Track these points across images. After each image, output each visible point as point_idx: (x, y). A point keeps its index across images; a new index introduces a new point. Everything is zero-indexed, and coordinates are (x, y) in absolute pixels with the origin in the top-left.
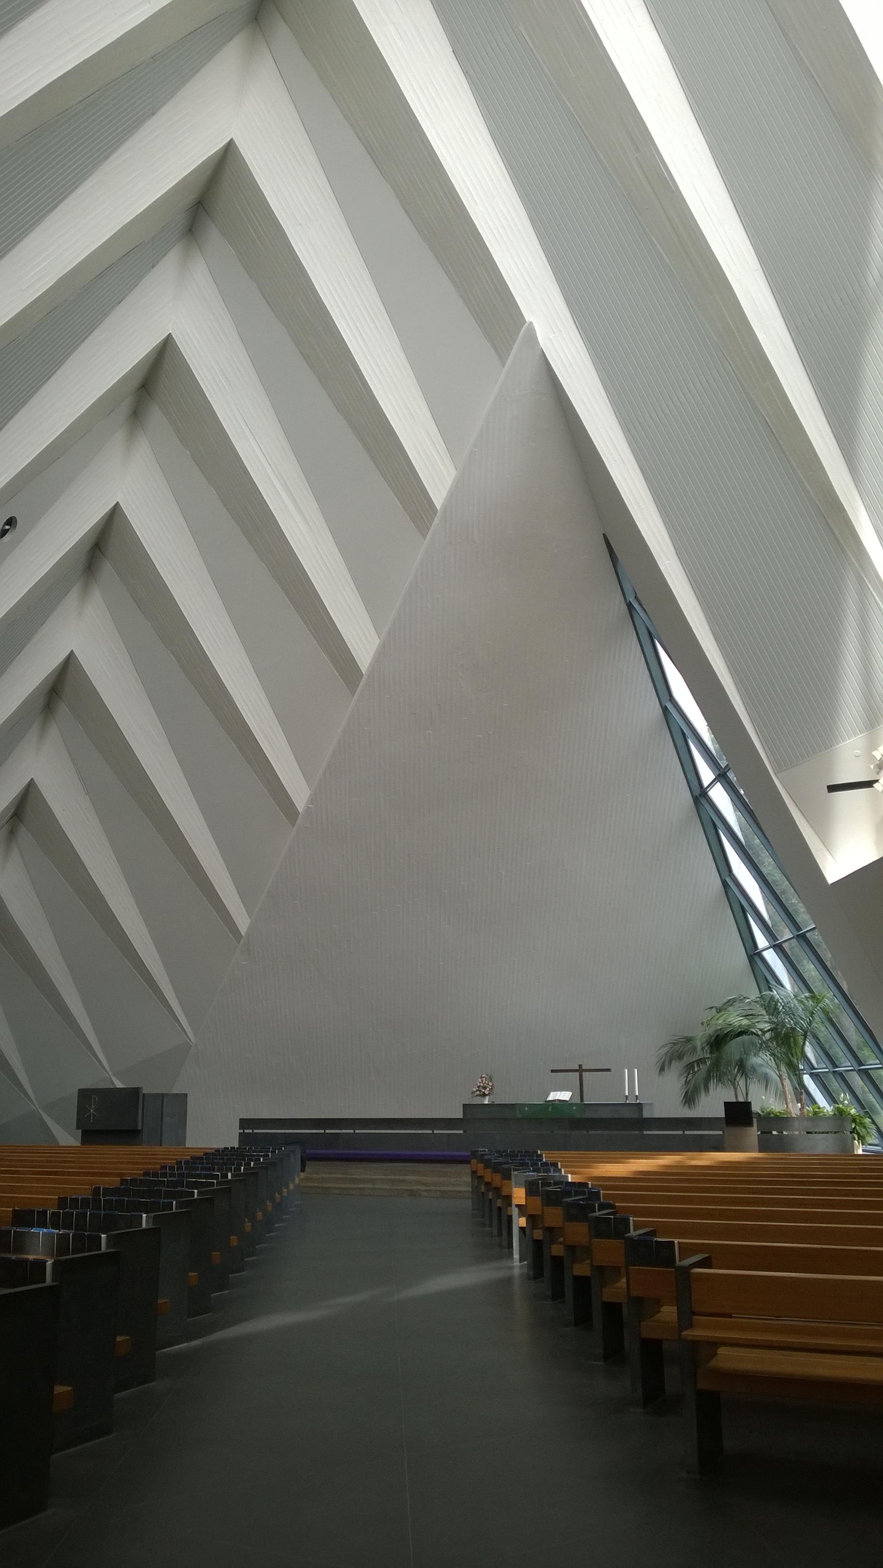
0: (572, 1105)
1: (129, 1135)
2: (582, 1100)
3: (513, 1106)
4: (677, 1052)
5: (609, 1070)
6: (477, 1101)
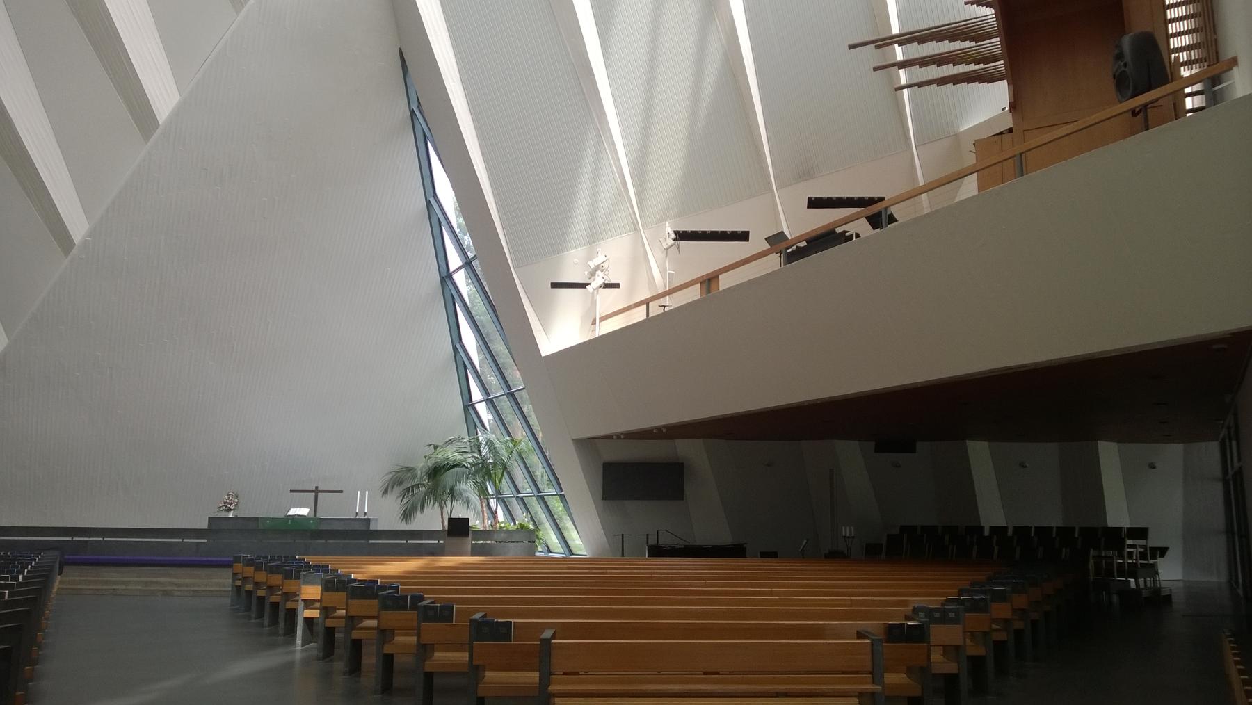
3: (257, 519)
4: (400, 481)
6: (223, 514)
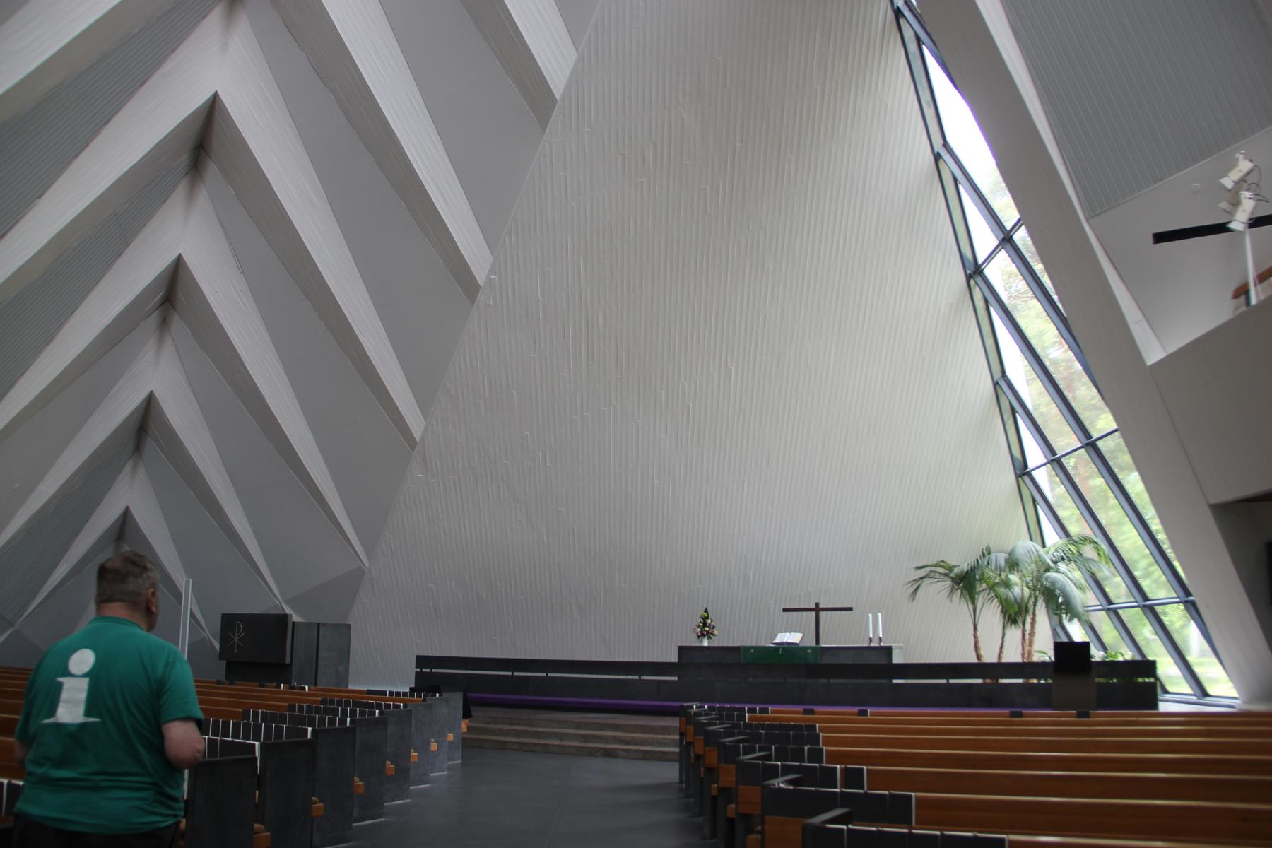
0: (806, 648)
1: (277, 670)
2: (818, 642)
3: (736, 649)
5: (850, 609)
